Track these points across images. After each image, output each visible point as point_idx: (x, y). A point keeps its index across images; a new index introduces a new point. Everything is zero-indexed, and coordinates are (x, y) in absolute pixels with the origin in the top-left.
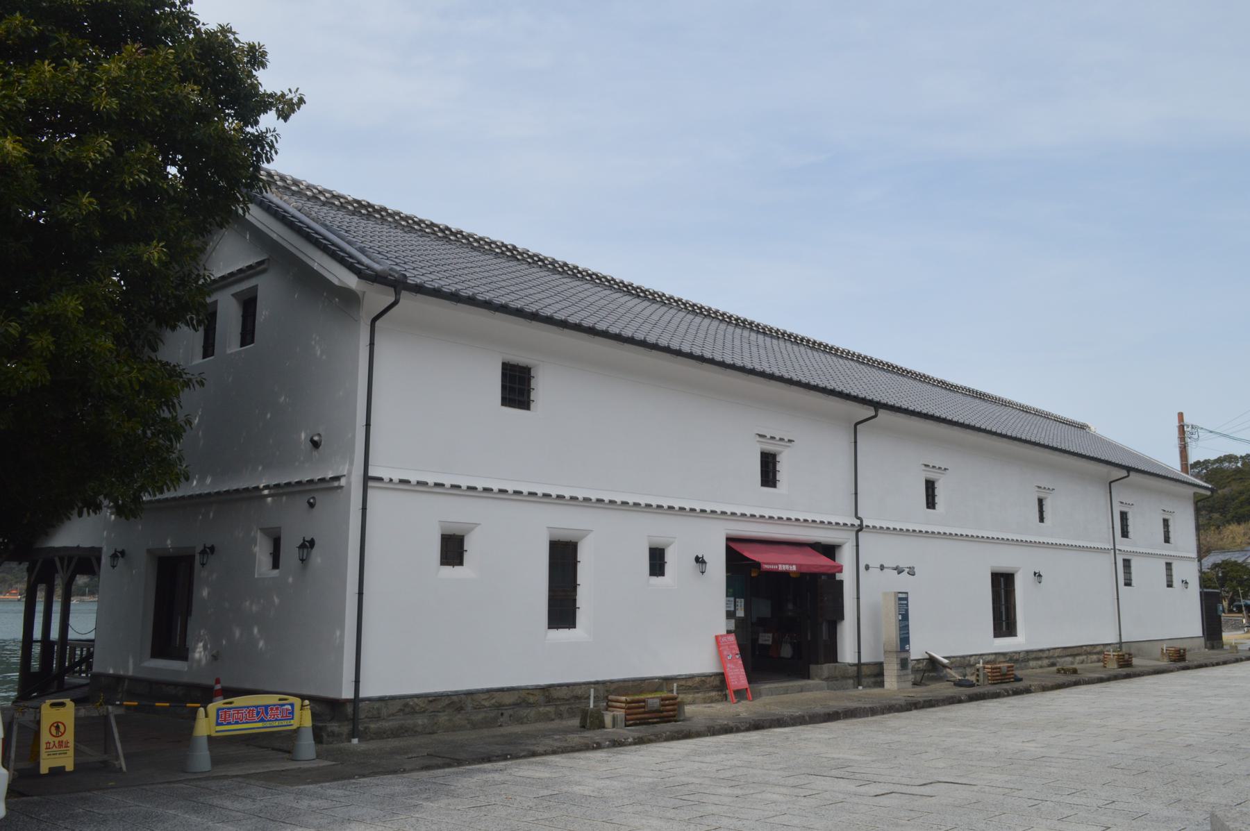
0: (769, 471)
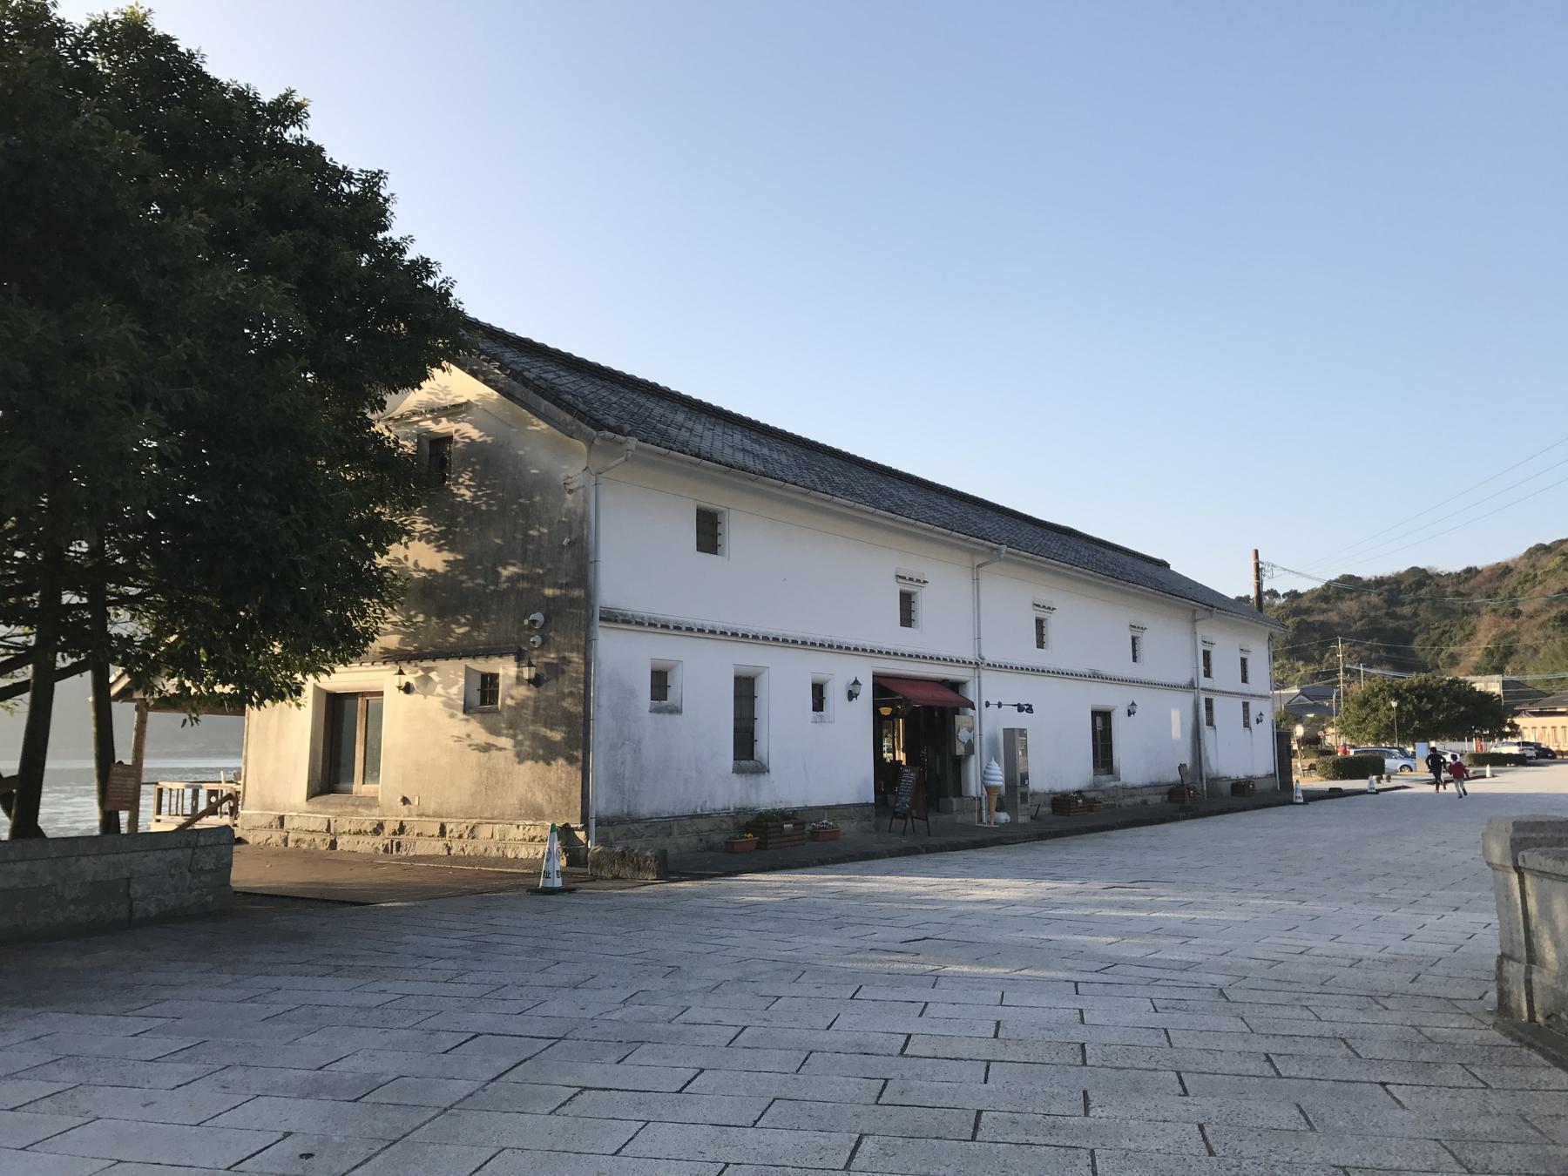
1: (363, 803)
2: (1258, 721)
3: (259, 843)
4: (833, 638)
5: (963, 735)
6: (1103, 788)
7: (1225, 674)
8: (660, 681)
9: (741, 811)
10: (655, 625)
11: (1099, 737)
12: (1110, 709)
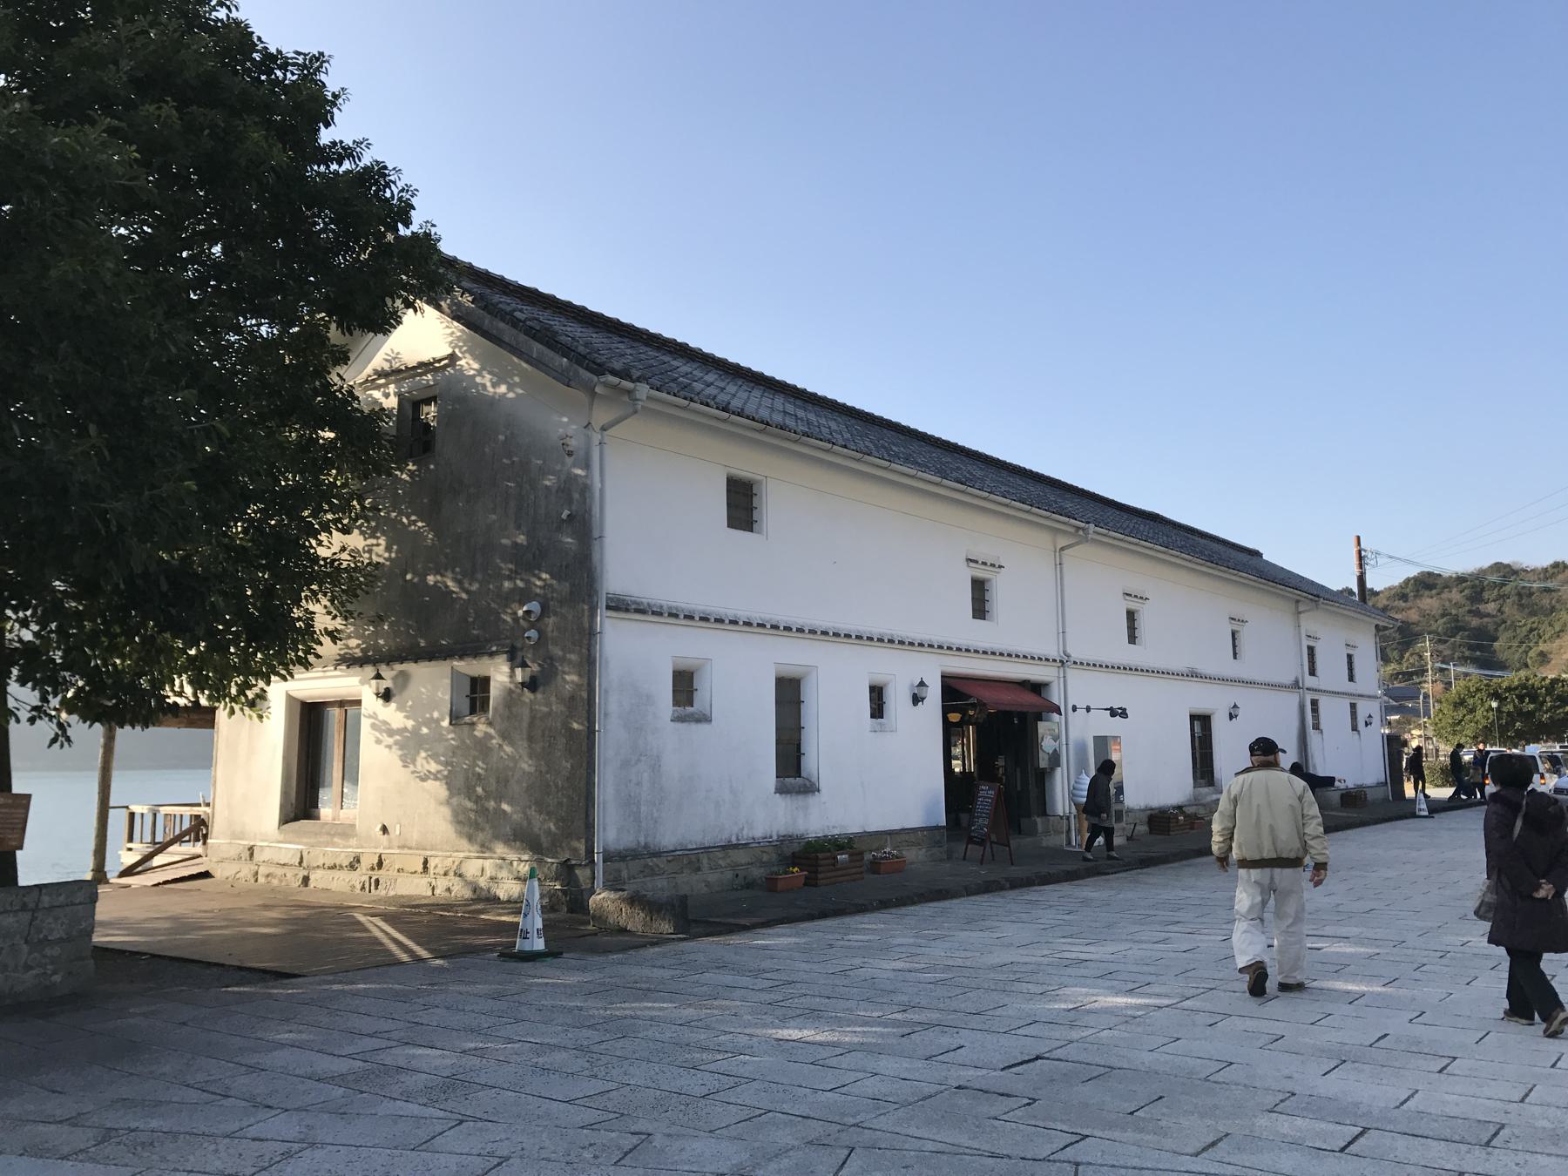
1: (339, 831)
2: (1367, 724)
3: (227, 878)
4: (894, 632)
5: (1047, 745)
6: (1203, 801)
7: (1331, 673)
8: (684, 684)
9: (786, 839)
11: (1197, 744)
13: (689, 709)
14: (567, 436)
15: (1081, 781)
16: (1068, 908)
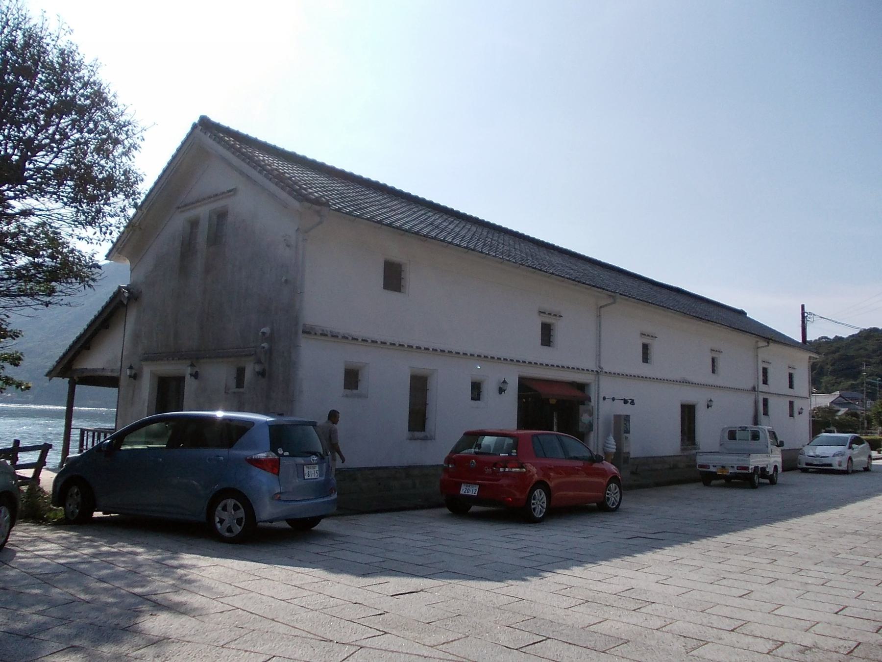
0: (547, 335)
2: (799, 413)
7: (778, 381)
10: (326, 335)
12: (694, 403)
13: (355, 391)
14: (286, 235)
15: (607, 442)
16: (771, 575)
